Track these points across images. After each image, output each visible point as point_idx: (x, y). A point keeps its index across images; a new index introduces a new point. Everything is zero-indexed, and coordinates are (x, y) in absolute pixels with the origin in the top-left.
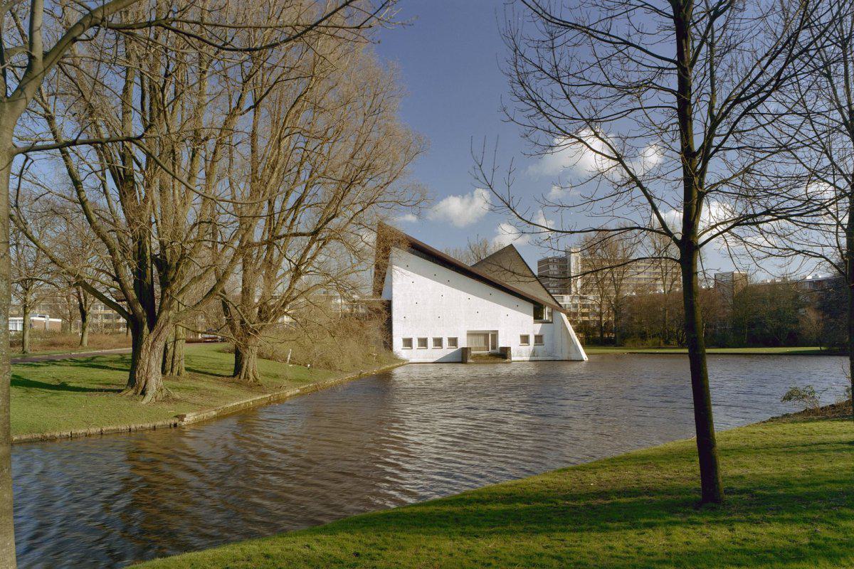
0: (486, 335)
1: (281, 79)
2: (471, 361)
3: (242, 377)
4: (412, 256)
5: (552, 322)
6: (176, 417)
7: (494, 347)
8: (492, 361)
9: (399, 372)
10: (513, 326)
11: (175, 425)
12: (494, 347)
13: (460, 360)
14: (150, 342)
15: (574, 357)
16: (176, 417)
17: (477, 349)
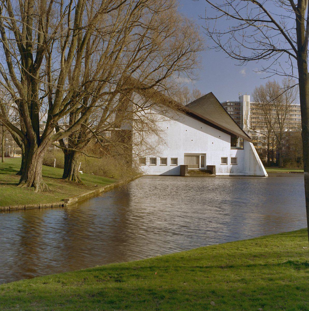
0: (197, 156)
2: (188, 175)
3: (71, 179)
5: (243, 149)
6: (63, 200)
8: (202, 175)
10: (217, 150)
11: (63, 206)
12: (203, 166)
13: (179, 175)
14: (38, 153)
15: (258, 173)
16: (63, 200)
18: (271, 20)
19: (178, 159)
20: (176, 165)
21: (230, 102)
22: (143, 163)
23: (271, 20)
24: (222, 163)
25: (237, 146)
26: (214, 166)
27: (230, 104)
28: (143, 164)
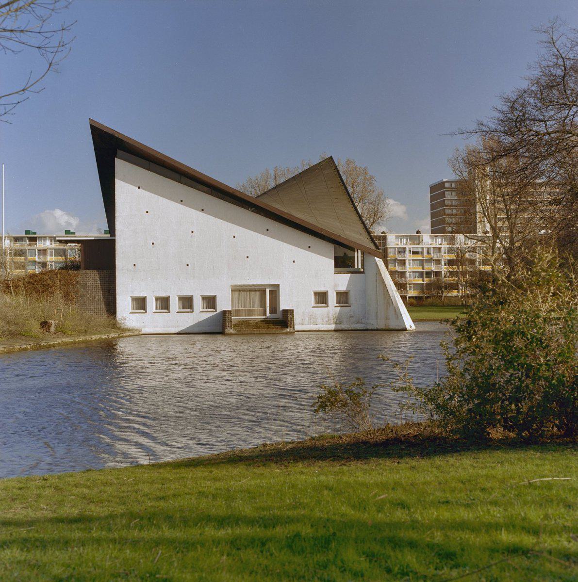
0: (261, 290)
1: (14, 105)
5: (363, 273)
7: (274, 310)
8: (265, 331)
9: (124, 346)
12: (274, 310)
15: (393, 324)
17: (240, 313)
19: (218, 299)
20: (212, 310)
21: (451, 182)
22: (142, 309)
24: (133, 309)
25: (356, 267)
26: (290, 310)
27: (451, 185)
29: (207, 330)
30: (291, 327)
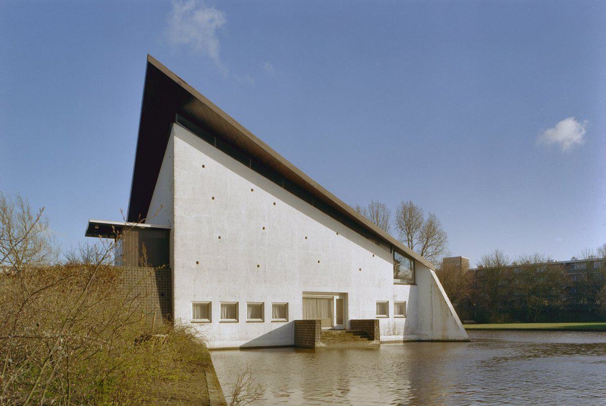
4: (217, 149)
12: (340, 321)
18: (188, 155)
20: (284, 319)
22: (206, 318)
23: (188, 155)
28: (257, 320)
29: (267, 343)
30: (377, 339)
